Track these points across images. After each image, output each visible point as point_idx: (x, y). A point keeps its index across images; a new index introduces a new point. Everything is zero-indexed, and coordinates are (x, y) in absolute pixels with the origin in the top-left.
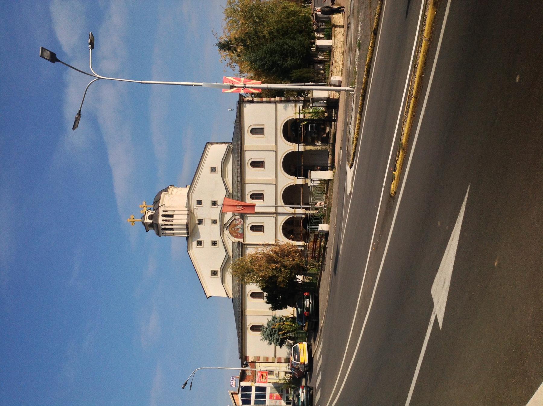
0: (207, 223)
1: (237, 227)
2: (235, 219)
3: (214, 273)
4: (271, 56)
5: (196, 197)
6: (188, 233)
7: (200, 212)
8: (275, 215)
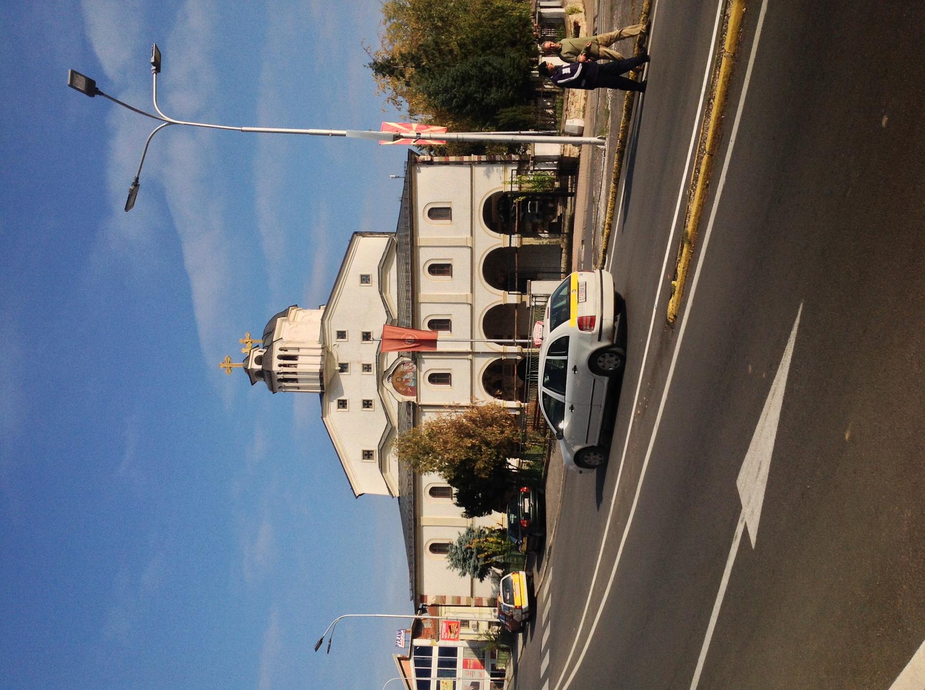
0: (355, 368)
1: (406, 377)
2: (403, 363)
3: (367, 455)
4: (463, 84)
5: (335, 326)
6: (322, 387)
7: (343, 352)
8: (470, 357)
